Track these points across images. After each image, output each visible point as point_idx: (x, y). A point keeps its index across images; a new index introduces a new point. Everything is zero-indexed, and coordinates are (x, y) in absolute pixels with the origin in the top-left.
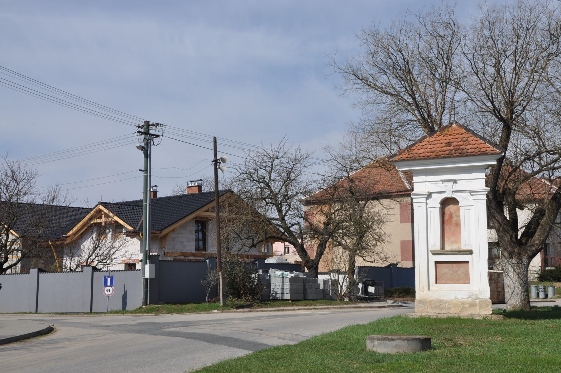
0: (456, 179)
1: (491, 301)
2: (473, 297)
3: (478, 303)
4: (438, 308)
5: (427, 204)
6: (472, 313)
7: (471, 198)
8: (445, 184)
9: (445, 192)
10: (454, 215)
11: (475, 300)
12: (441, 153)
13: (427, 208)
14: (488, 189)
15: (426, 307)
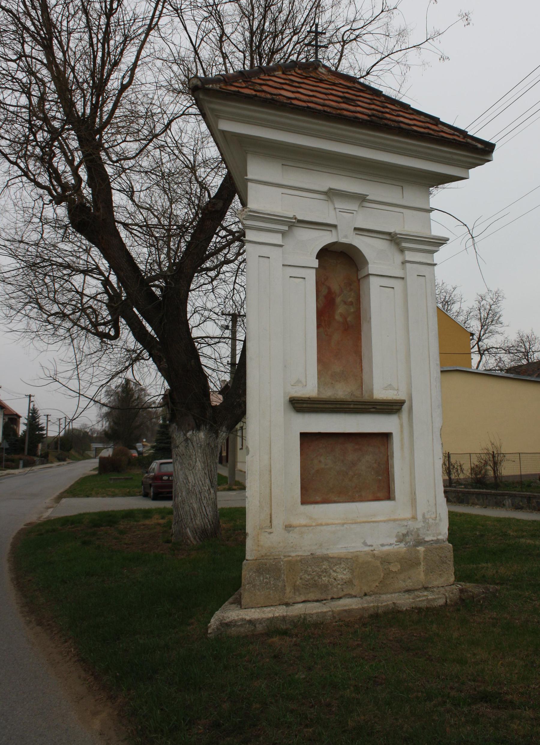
3: (422, 557)
8: (340, 204)
10: (338, 300)
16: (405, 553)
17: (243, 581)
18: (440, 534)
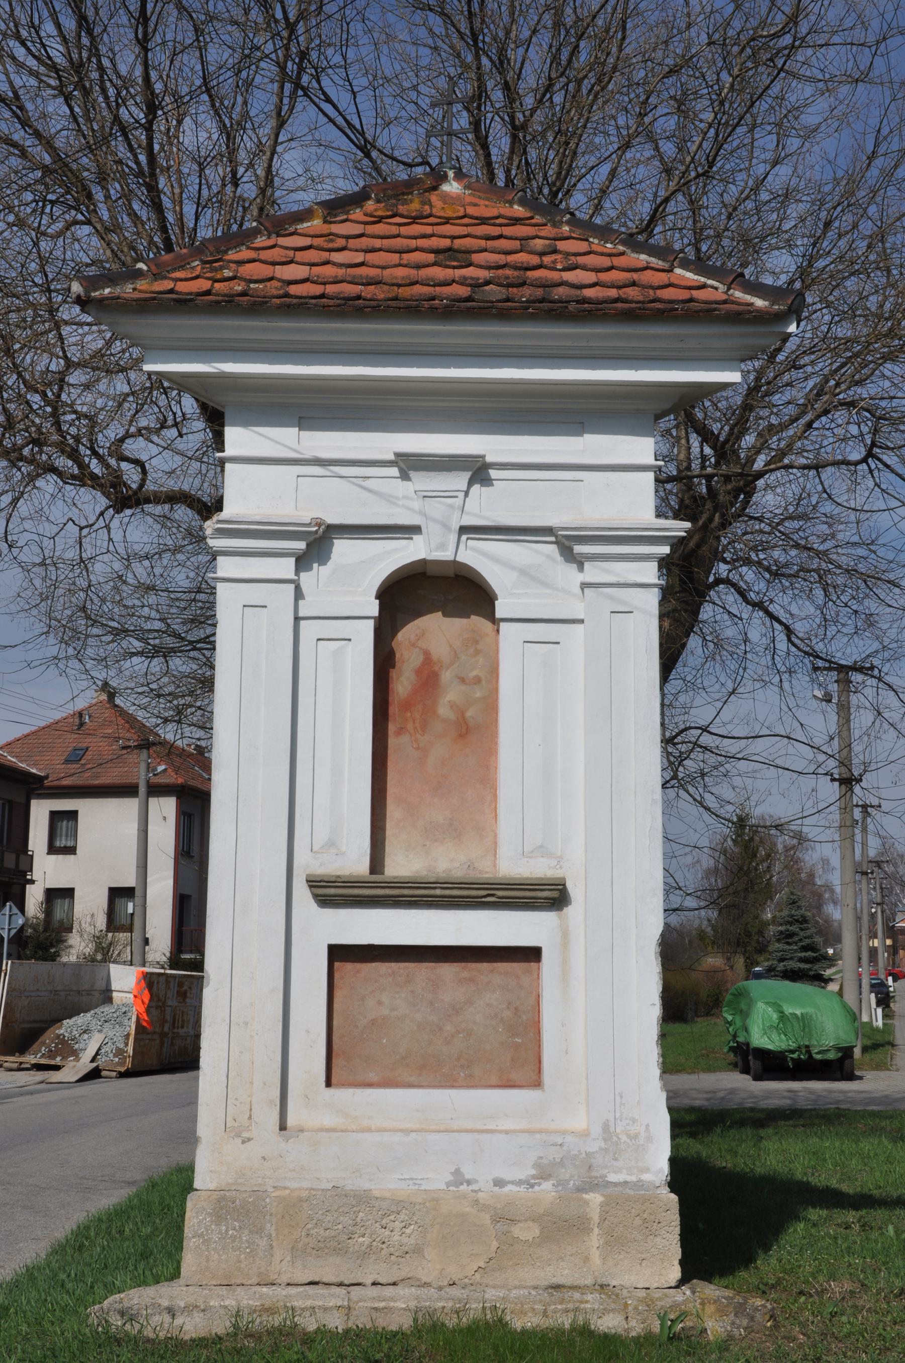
0: (489, 459)
1: (674, 1197)
2: (564, 1173)
3: (595, 1216)
4: (340, 1250)
5: (299, 594)
6: (555, 1281)
7: (571, 576)
8: (423, 481)
9: (415, 530)
10: (446, 676)
11: (580, 1190)
12: (418, 289)
13: (297, 619)
14: (680, 527)
15: (263, 1243)
16: (552, 1203)
17: (186, 1230)
18: (647, 1170)
